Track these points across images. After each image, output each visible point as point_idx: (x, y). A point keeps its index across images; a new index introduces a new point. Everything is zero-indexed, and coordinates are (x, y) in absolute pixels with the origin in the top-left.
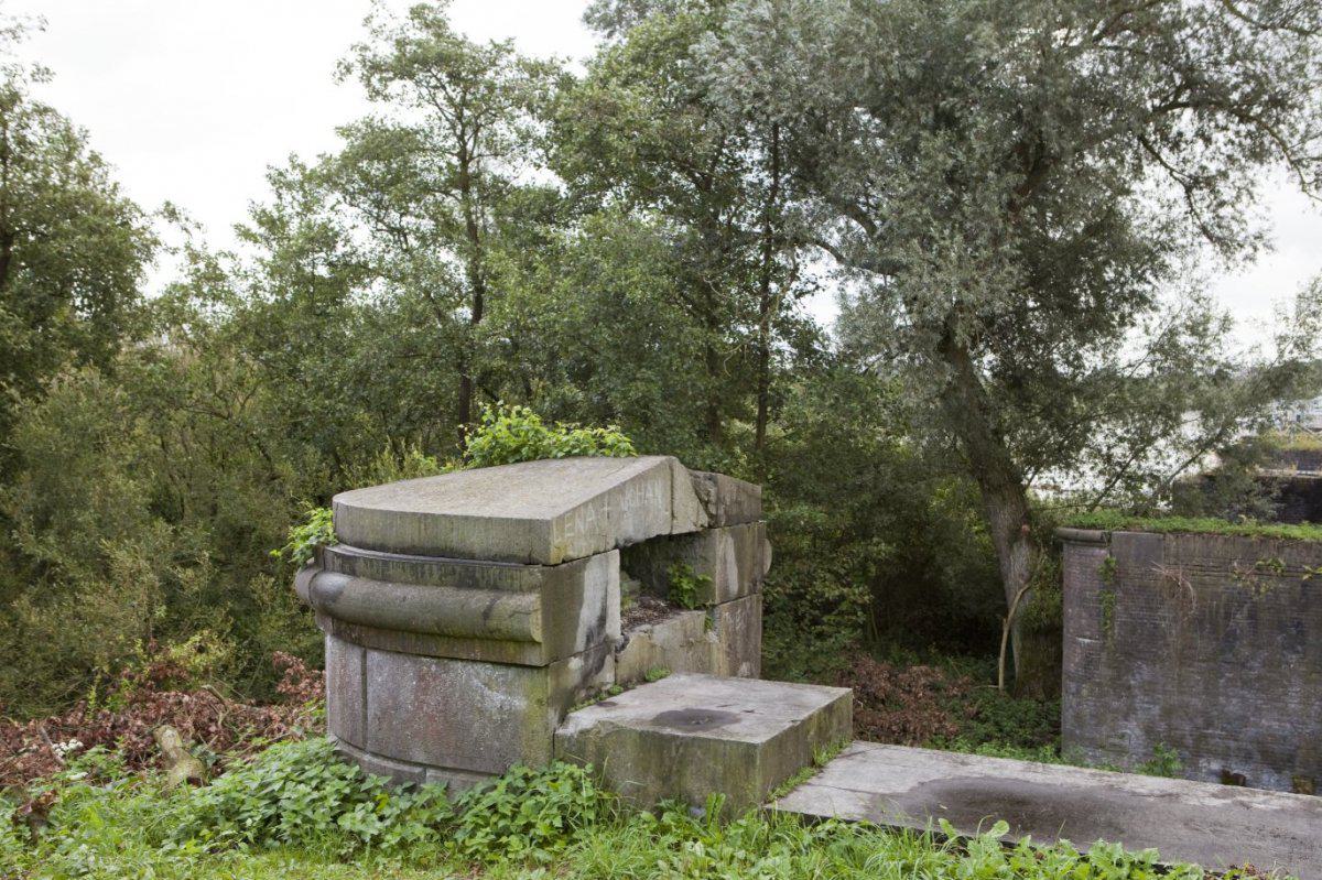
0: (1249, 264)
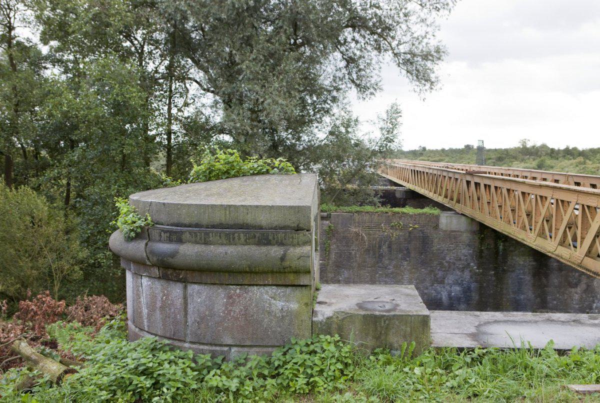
0: (373, 97)
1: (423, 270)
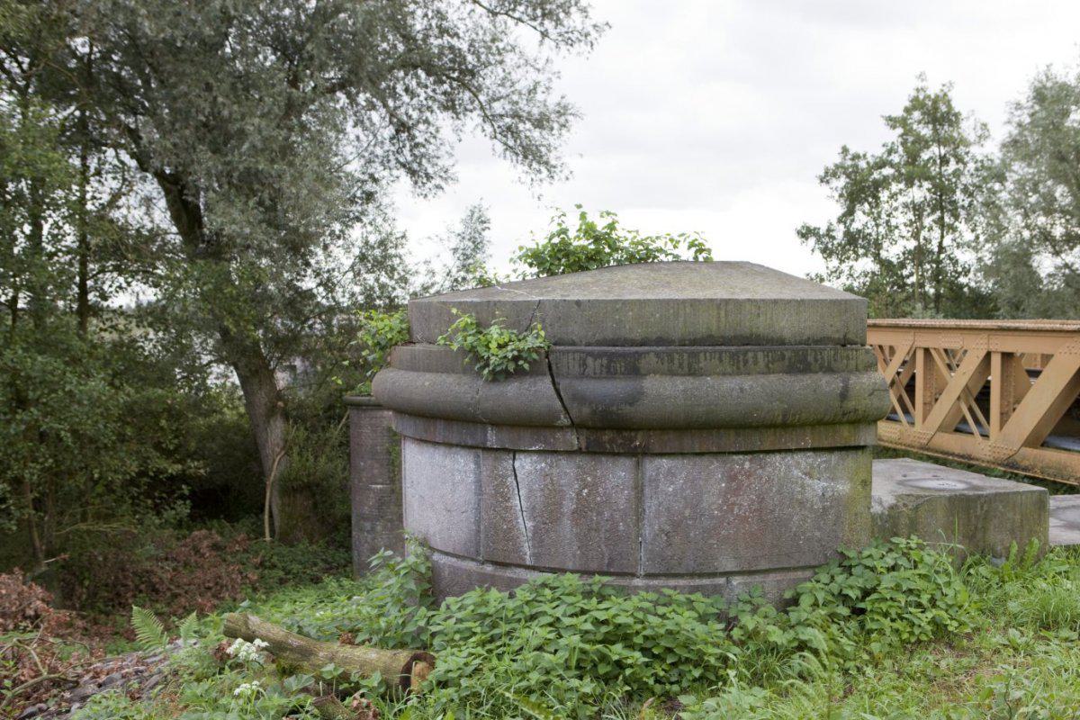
0: (440, 192)
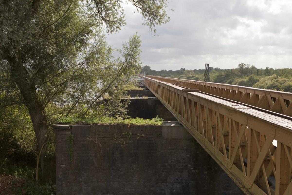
1: (149, 171)
